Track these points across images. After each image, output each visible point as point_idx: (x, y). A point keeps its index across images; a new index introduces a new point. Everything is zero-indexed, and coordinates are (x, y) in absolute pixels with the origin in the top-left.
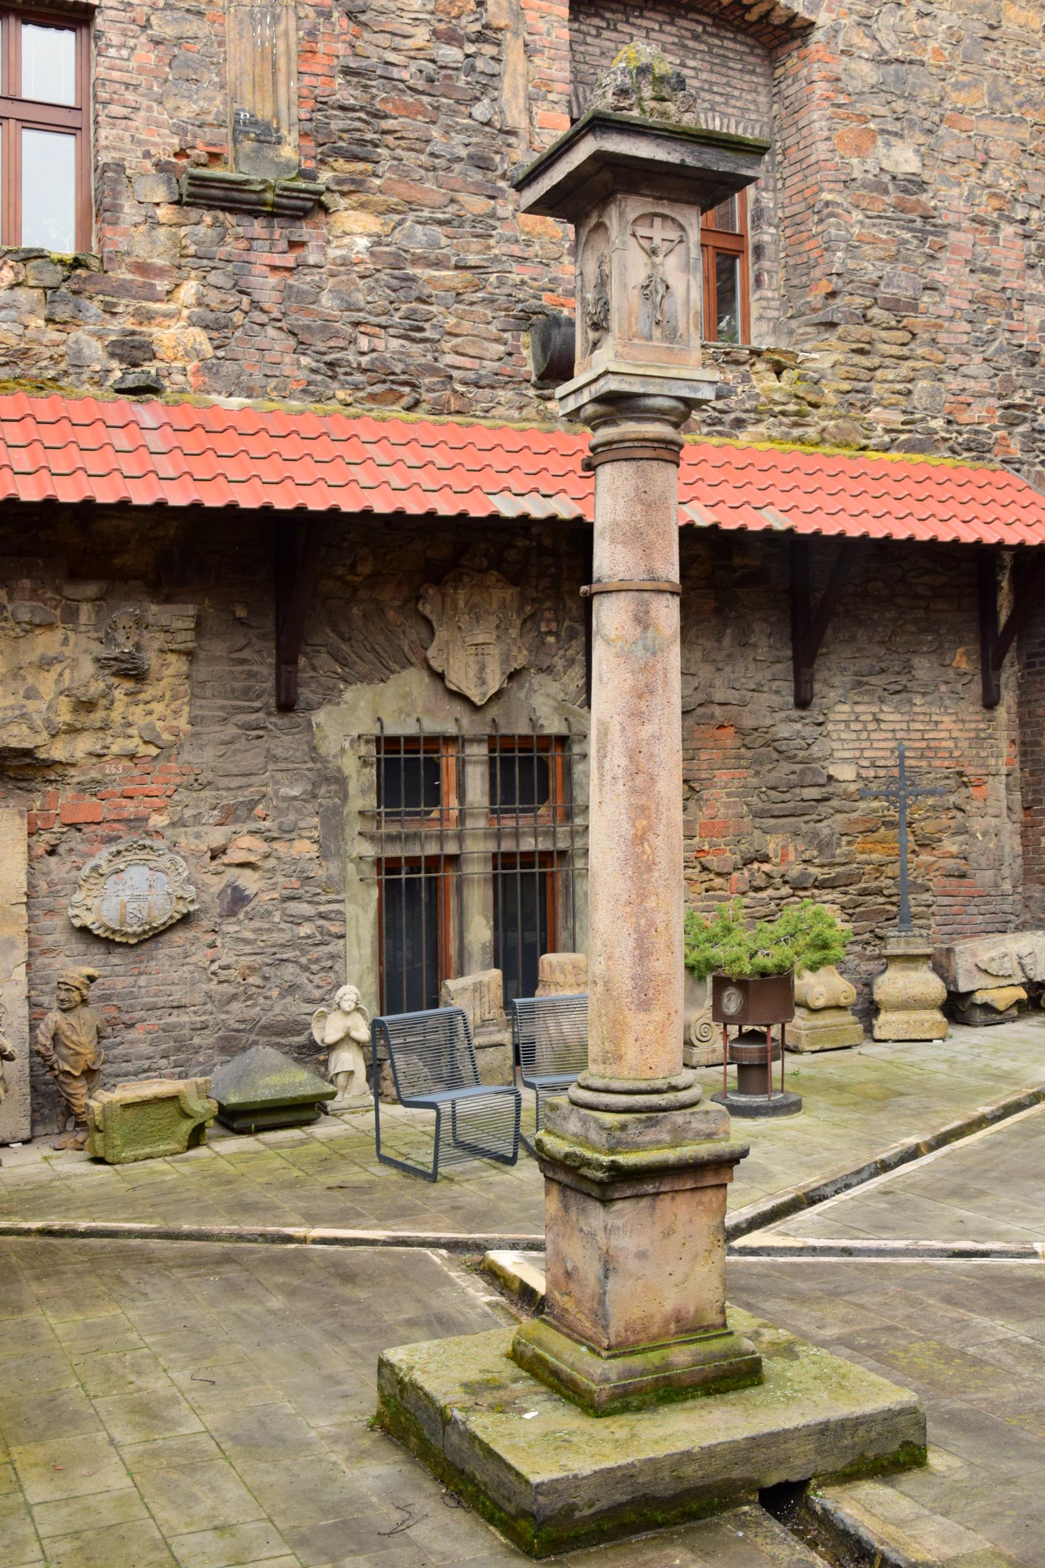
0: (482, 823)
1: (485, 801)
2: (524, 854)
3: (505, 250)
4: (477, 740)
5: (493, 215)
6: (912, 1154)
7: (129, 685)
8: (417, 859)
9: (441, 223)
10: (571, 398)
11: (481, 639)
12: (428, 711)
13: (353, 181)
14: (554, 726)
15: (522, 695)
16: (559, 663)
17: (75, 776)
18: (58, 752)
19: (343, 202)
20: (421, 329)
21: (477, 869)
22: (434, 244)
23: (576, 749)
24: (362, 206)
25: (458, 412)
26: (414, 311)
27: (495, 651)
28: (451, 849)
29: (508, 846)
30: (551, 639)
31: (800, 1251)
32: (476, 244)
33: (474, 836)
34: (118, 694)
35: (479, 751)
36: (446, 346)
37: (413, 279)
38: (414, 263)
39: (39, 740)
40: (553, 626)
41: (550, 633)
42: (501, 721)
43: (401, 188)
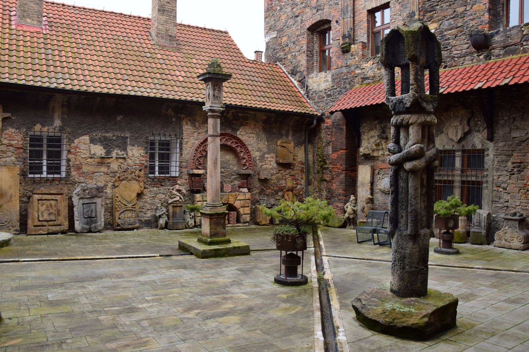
0: (459, 172)
1: (460, 167)
2: (468, 181)
3: (468, 18)
4: (458, 151)
5: (466, 10)
6: (479, 268)
7: (384, 141)
8: (441, 180)
9: (452, 18)
10: (43, 198)
11: (455, 125)
12: (447, 144)
13: (430, 17)
14: (479, 147)
15: (471, 138)
16: (481, 129)
17: (380, 159)
18: (375, 154)
19: (429, 23)
20: (447, 47)
21: (457, 184)
22: (451, 24)
23: (486, 153)
24: (433, 22)
25: (455, 66)
26: (445, 43)
27: (460, 127)
28: (450, 178)
29: (464, 179)
30: (479, 123)
31: (380, 261)
32: (461, 20)
33: (457, 176)
34: (383, 142)
35: (459, 154)
36: (453, 50)
37: (445, 35)
38: (445, 31)
39: (370, 152)
40: (480, 119)
41: (478, 121)
42: (465, 146)
43: (442, 14)
